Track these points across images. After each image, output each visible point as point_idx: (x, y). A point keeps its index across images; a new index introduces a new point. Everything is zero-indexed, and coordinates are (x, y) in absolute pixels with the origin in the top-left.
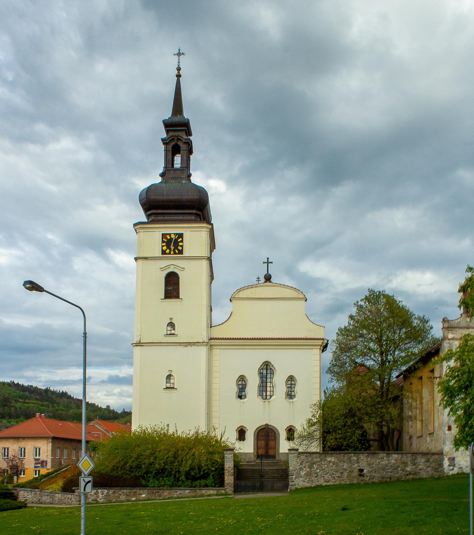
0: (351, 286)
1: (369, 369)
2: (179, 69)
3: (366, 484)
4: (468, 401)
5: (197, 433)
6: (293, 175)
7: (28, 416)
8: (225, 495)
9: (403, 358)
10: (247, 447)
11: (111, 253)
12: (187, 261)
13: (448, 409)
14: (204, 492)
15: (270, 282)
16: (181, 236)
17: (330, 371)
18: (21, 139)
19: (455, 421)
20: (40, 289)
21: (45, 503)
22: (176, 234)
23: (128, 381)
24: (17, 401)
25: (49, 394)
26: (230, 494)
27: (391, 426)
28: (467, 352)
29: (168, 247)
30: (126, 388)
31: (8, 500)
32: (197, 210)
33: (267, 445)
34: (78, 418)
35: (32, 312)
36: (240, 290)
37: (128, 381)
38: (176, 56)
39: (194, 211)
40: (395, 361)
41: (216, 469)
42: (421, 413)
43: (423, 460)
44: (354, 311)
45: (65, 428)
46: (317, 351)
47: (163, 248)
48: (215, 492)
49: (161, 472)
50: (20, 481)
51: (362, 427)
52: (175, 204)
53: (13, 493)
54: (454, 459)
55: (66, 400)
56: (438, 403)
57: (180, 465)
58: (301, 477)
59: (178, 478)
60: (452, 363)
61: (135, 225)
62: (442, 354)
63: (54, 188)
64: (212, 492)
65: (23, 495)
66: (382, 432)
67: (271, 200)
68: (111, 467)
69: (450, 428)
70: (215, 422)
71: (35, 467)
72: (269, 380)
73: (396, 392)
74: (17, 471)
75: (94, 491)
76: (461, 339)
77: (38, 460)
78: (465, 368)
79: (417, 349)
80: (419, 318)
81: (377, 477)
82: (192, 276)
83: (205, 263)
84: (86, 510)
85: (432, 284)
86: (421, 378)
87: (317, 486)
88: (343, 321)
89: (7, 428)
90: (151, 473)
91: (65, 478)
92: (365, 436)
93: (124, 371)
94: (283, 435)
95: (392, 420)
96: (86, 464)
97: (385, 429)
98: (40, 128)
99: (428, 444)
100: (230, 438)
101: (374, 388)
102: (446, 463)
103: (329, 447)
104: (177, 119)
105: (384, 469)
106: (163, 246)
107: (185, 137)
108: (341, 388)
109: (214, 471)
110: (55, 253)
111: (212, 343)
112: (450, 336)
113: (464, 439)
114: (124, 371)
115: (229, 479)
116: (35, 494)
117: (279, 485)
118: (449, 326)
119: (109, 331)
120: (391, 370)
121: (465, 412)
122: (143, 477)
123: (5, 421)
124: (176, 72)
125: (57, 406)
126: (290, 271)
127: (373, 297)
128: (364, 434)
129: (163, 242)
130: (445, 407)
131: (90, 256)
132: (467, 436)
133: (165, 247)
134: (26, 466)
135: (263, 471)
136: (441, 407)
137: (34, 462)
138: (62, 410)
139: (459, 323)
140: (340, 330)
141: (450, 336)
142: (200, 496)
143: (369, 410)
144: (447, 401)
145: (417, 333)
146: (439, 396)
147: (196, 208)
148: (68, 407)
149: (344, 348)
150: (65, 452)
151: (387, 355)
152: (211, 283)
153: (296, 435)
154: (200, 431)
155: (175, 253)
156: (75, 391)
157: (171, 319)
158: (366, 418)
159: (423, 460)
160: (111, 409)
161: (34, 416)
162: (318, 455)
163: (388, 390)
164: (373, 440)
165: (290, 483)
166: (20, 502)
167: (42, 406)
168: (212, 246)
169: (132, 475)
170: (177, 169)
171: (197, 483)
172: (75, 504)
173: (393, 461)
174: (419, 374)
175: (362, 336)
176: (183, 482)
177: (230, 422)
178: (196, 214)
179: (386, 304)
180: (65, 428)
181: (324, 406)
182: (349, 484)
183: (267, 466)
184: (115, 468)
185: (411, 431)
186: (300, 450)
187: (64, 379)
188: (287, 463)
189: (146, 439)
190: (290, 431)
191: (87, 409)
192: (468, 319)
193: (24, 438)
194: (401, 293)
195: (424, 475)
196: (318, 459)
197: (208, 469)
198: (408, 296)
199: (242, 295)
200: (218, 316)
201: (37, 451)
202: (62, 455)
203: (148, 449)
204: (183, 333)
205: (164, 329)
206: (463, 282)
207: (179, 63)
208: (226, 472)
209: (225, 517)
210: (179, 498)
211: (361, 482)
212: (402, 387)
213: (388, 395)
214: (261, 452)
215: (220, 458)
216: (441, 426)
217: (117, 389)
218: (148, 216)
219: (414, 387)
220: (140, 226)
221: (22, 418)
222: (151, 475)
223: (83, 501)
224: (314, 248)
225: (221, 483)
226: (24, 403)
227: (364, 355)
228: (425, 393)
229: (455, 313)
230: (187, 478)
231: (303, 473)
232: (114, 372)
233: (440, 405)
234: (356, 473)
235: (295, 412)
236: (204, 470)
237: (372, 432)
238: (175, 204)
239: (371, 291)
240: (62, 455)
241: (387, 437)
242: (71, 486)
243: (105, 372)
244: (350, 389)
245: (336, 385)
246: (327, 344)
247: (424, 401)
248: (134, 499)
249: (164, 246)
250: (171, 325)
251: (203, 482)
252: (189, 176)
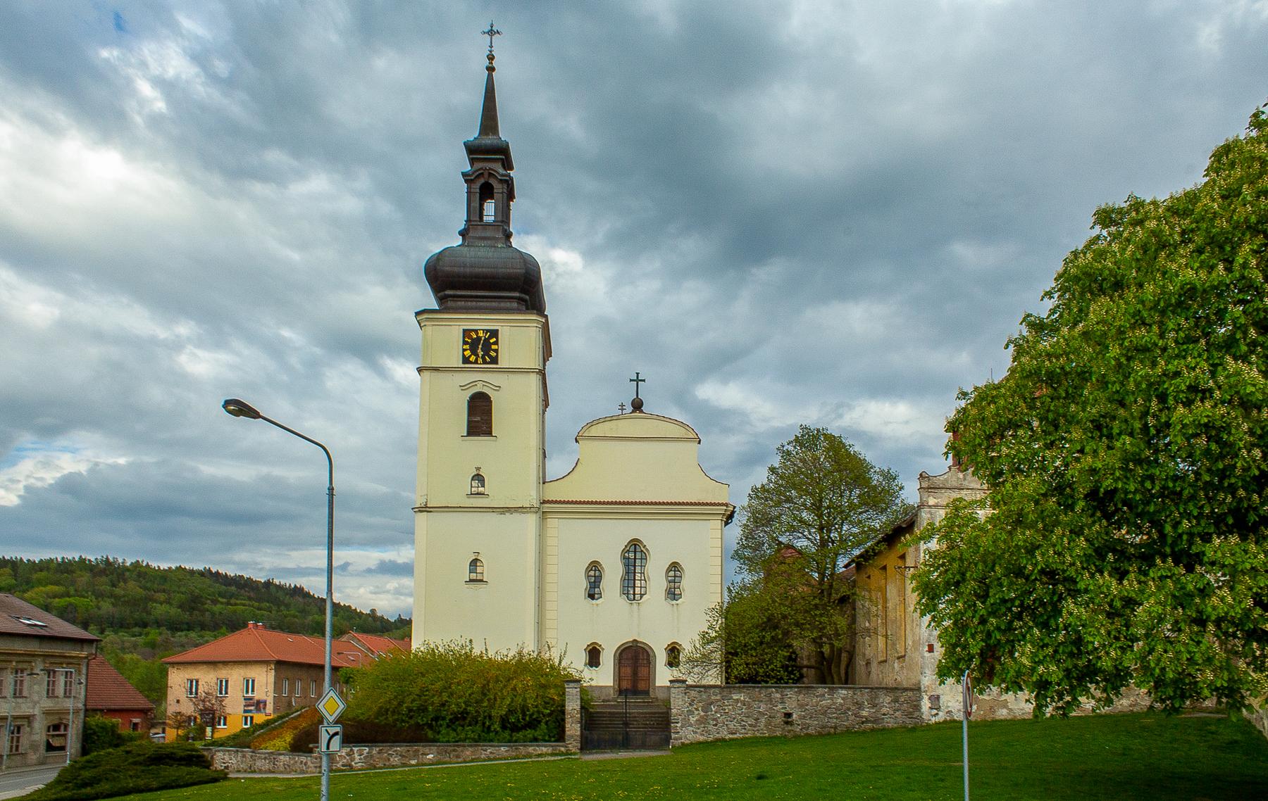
0: (777, 424)
1: (800, 552)
2: (491, 58)
3: (797, 737)
4: (960, 604)
5: (520, 653)
6: (692, 246)
7: (236, 625)
8: (567, 754)
9: (855, 535)
10: (603, 677)
11: (388, 363)
12: (505, 375)
13: (928, 617)
14: (530, 749)
15: (642, 412)
16: (494, 333)
17: (737, 555)
18: (238, 174)
19: (940, 637)
20: (253, 414)
21: (261, 771)
23: (405, 570)
24: (215, 602)
25: (273, 589)
26: (575, 754)
27: (836, 643)
28: (959, 526)
29: (474, 352)
30: (407, 582)
31: (194, 769)
32: (521, 292)
33: (635, 673)
34: (319, 629)
35: (253, 456)
36: (591, 424)
37: (405, 570)
39: (517, 294)
40: (843, 541)
41: (552, 712)
42: (885, 624)
43: (888, 699)
44: (776, 462)
45: (297, 647)
46: (717, 524)
48: (550, 750)
49: (460, 718)
50: (217, 735)
51: (790, 646)
52: (484, 284)
53: (203, 756)
54: (938, 697)
55: (300, 599)
56: (912, 608)
57: (492, 707)
58: (691, 725)
59: (489, 727)
60: (934, 545)
61: (418, 314)
62: (917, 531)
63: (296, 256)
64: (544, 749)
65: (221, 759)
66: (822, 653)
67: (656, 284)
68: (375, 709)
69: (931, 649)
70: (550, 636)
71: (245, 711)
72: (638, 569)
73: (844, 591)
74: (213, 718)
75: (344, 751)
76: (947, 505)
77: (251, 699)
78: (956, 553)
79: (878, 522)
80: (882, 473)
81: (814, 725)
82: (514, 399)
83: (534, 380)
84: (329, 779)
85: (907, 422)
86: (884, 568)
87: (717, 740)
88: (761, 477)
89: (197, 645)
90: (444, 719)
91: (296, 728)
92: (795, 660)
93: (403, 555)
94: (661, 658)
95: (837, 634)
96: (331, 705)
97: (826, 649)
98: (275, 157)
99: (896, 674)
100: (575, 662)
101: (809, 584)
102: (926, 704)
103: (736, 677)
104: (489, 140)
105: (825, 713)
106: (464, 350)
107: (501, 171)
108: (756, 584)
109: (550, 715)
110: (294, 361)
111: (545, 509)
112: (932, 501)
113: (956, 666)
114: (403, 555)
115: (573, 728)
116: (244, 756)
117: (655, 738)
118: (929, 484)
119: (382, 489)
120: (837, 555)
121: (955, 623)
122: (430, 727)
123: (192, 635)
125: (287, 608)
126: (681, 398)
127: (809, 439)
128: (793, 658)
129: (465, 343)
130: (923, 614)
131: (353, 367)
132: (959, 660)
134: (228, 710)
135: (629, 716)
136: (917, 615)
137: (243, 703)
138: (295, 616)
139: (946, 480)
140: (755, 490)
141: (932, 501)
142: (525, 757)
143: (800, 617)
144: (927, 605)
145: (878, 495)
146: (912, 598)
147: (522, 289)
148: (303, 612)
149: (760, 519)
150: (299, 685)
151: (829, 531)
152: (544, 412)
153: (682, 658)
154: (525, 651)
155: (485, 362)
156: (315, 586)
157: (478, 469)
158: (796, 631)
159: (888, 699)
160: (379, 614)
161: (245, 625)
162: (717, 691)
163: (831, 586)
164: (808, 667)
165: (673, 736)
166: (216, 771)
167: (259, 609)
168: (547, 352)
169: (412, 722)
170: (488, 225)
171: (520, 735)
172: (312, 772)
173: (840, 701)
174: (881, 562)
175: (789, 500)
176: (497, 732)
177: (575, 637)
178: (520, 300)
179: (828, 450)
180: (297, 647)
181: (727, 612)
182: (769, 738)
183: (635, 706)
184: (383, 712)
185: (869, 652)
186: (690, 682)
187: (304, 566)
188: (667, 703)
189: (434, 663)
190: (674, 652)
191: (335, 614)
192: (961, 475)
193: (225, 663)
194: (859, 435)
195: (890, 723)
196: (718, 697)
197: (538, 712)
198: (871, 440)
199: (594, 431)
200: (556, 467)
201: (249, 684)
202: (292, 691)
203: (439, 679)
204: (497, 493)
205: (466, 485)
206: (952, 415)
208: (567, 716)
209: (564, 790)
210: (490, 760)
211: (787, 734)
212: (854, 581)
213: (830, 594)
214: (626, 685)
215: (559, 695)
216: (917, 644)
217: (393, 583)
218: (441, 300)
219: (873, 583)
220: (426, 316)
221: (224, 629)
222: (444, 723)
223: (324, 767)
224: (721, 362)
225: (559, 734)
226: (228, 604)
227: (792, 529)
228: (892, 591)
229: (940, 465)
230: (504, 727)
231: (693, 719)
232: (389, 555)
233: (915, 610)
234: (779, 719)
235: (682, 621)
236: (531, 716)
237: (805, 653)
238: (484, 284)
239: (803, 428)
240: (292, 691)
241: (830, 662)
242: (304, 743)
243: (374, 556)
244: (770, 585)
245: (748, 578)
246: (733, 512)
247: (890, 605)
248: (413, 762)
250: (479, 478)
251: (529, 733)
252: (508, 236)
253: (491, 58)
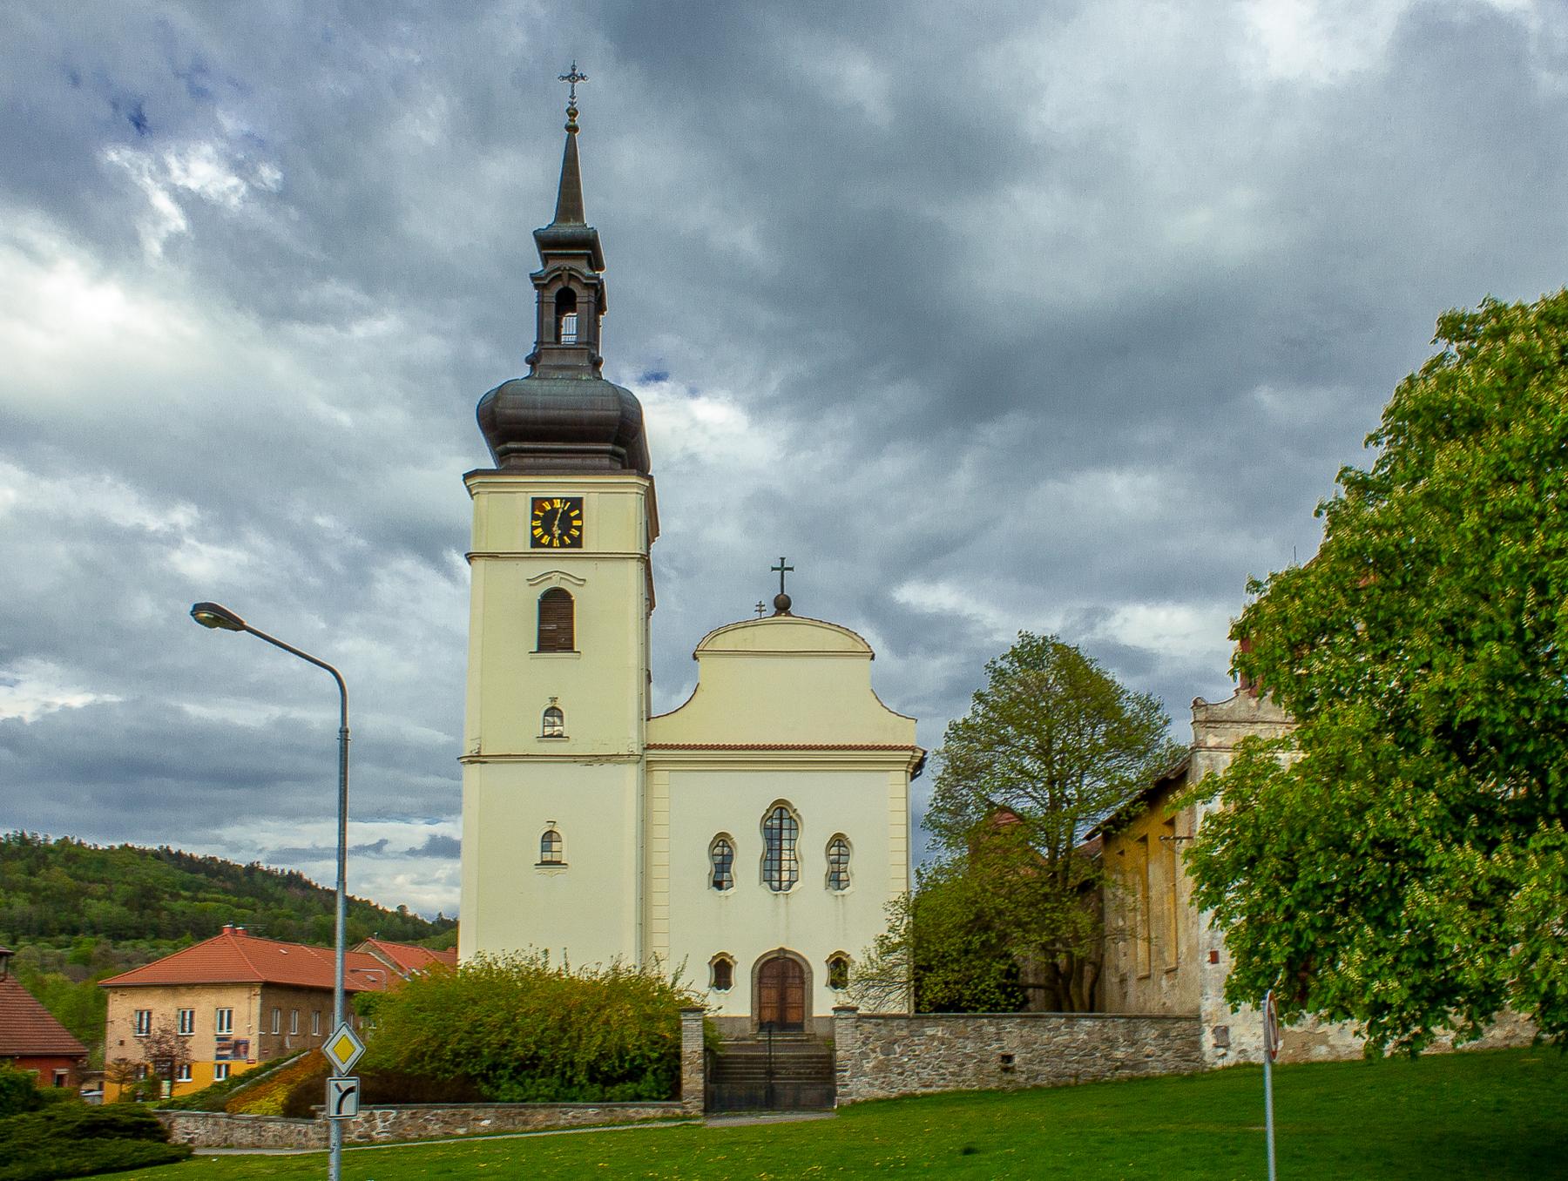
16: (577, 503)
48: (659, 1113)
129: (535, 517)
253: (573, 113)
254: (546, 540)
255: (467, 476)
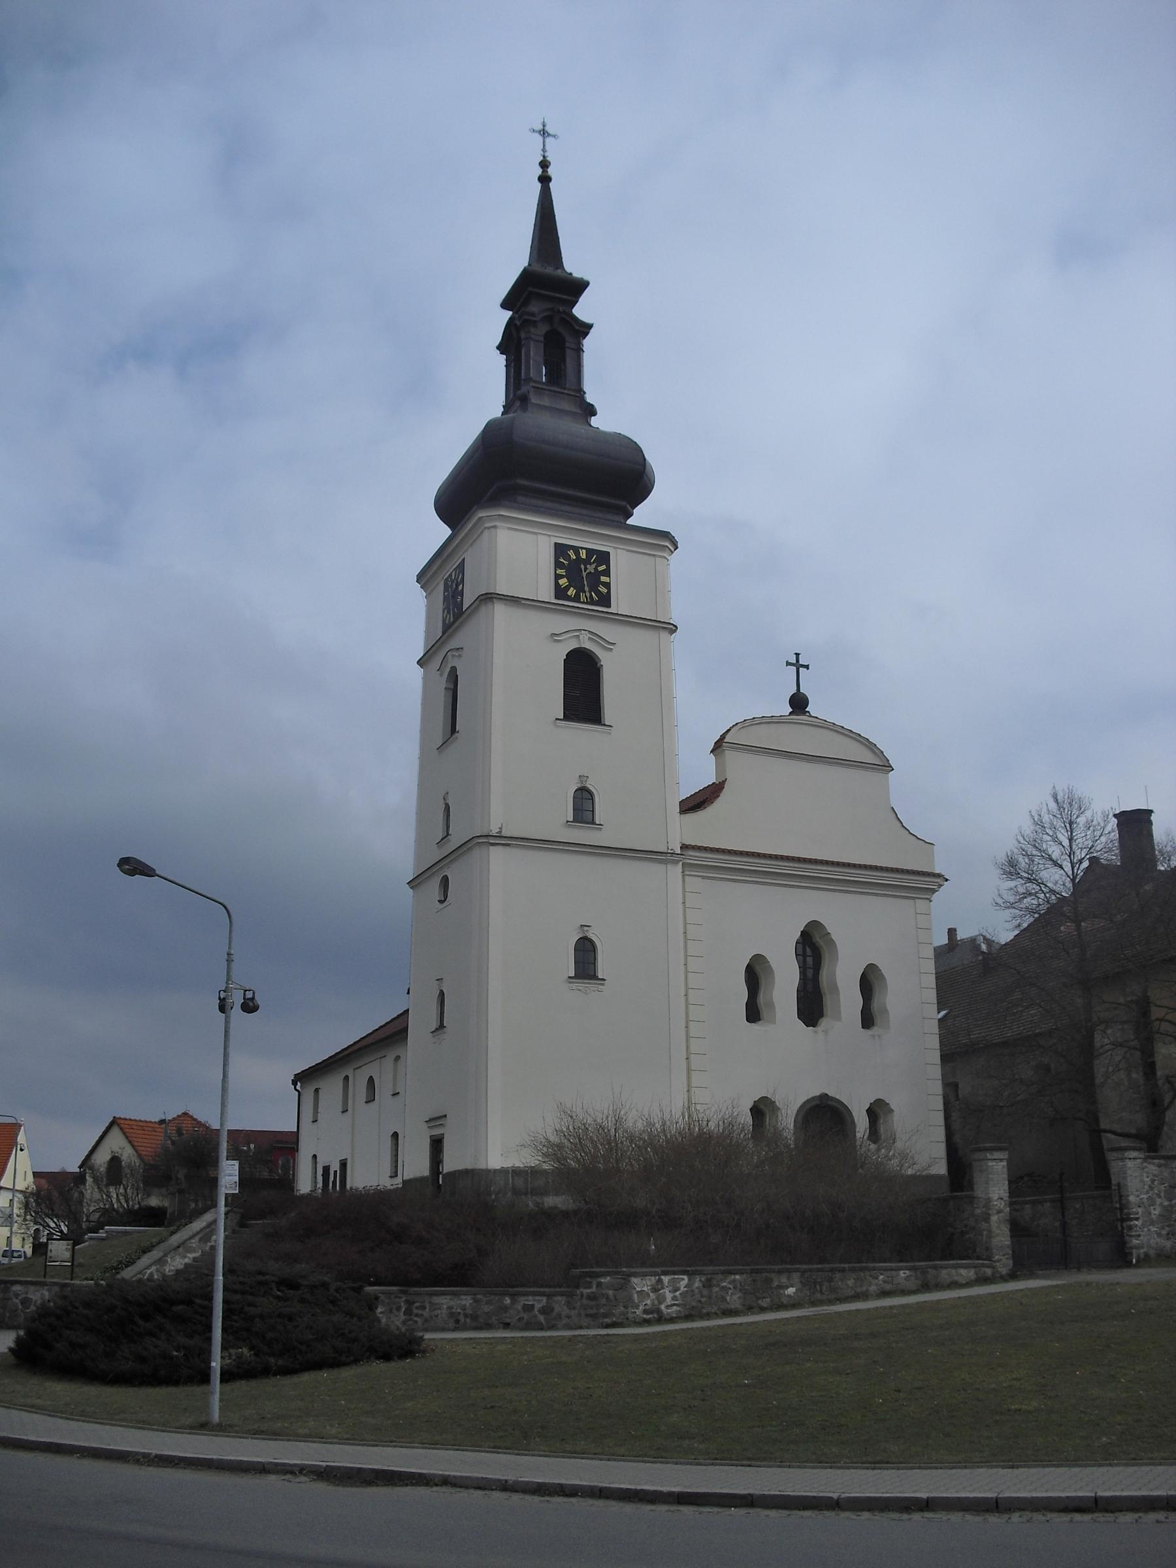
2: (544, 164)
16: (604, 557)
22: (590, 552)
38: (537, 135)
47: (561, 582)
48: (971, 1274)
124: (539, 171)
129: (558, 565)
133: (565, 580)
207: (544, 150)
234: (383, 1089)
249: (562, 577)
254: (572, 592)
255: (302, 1078)
